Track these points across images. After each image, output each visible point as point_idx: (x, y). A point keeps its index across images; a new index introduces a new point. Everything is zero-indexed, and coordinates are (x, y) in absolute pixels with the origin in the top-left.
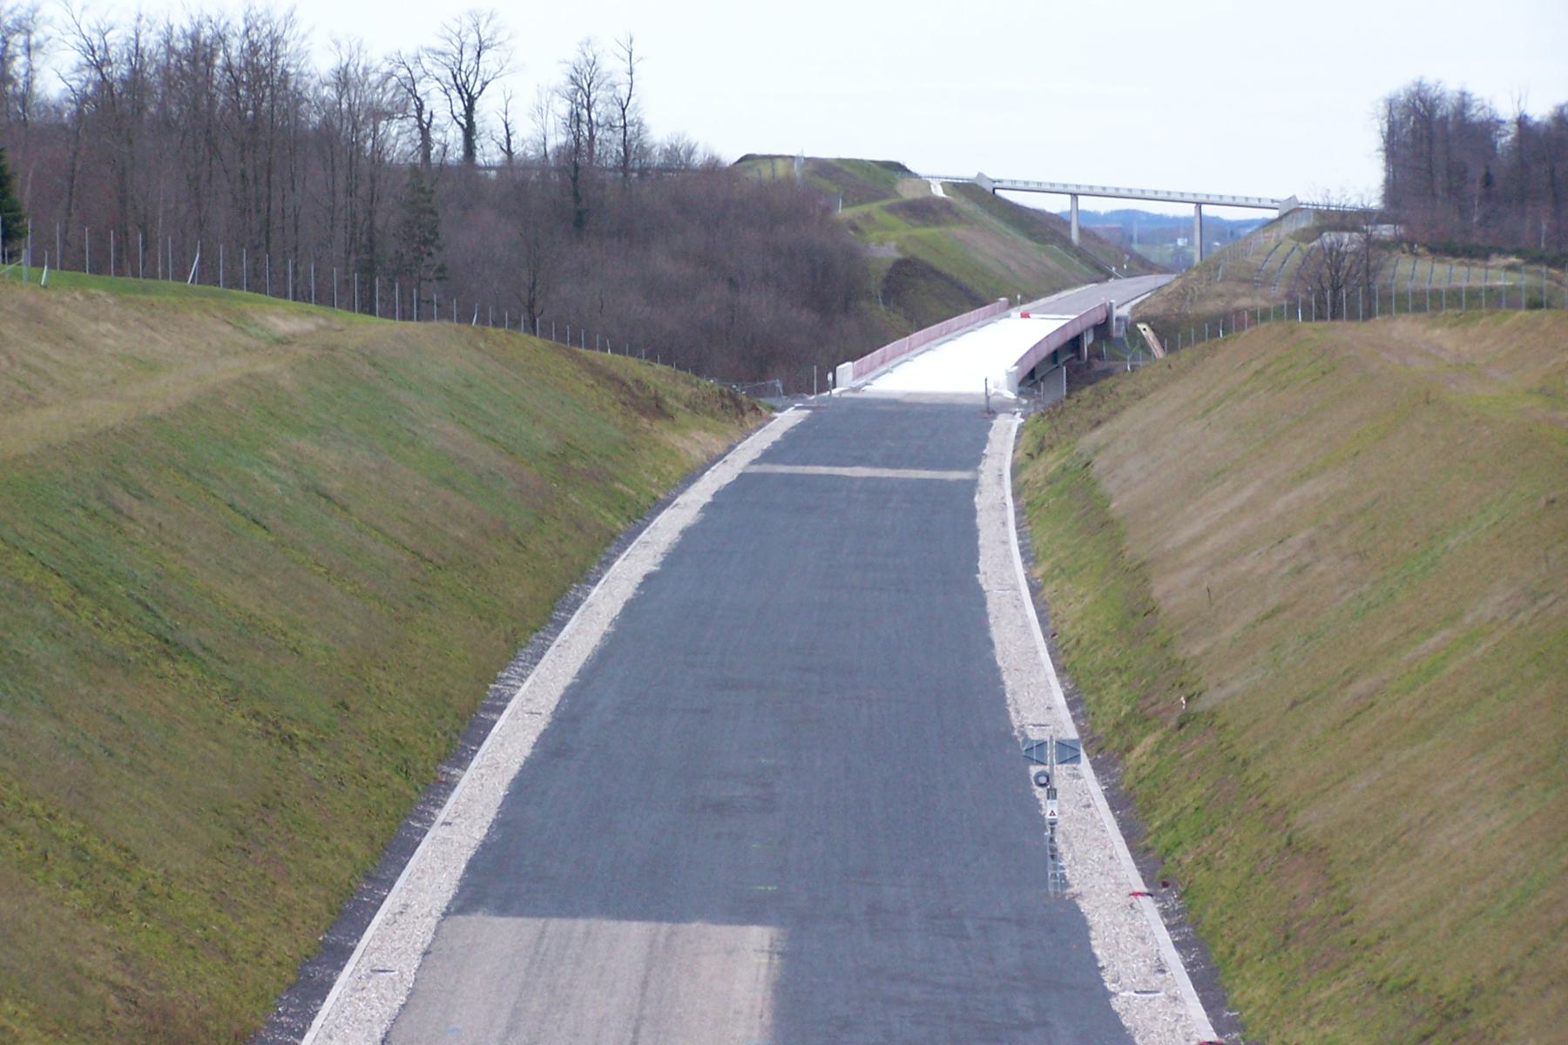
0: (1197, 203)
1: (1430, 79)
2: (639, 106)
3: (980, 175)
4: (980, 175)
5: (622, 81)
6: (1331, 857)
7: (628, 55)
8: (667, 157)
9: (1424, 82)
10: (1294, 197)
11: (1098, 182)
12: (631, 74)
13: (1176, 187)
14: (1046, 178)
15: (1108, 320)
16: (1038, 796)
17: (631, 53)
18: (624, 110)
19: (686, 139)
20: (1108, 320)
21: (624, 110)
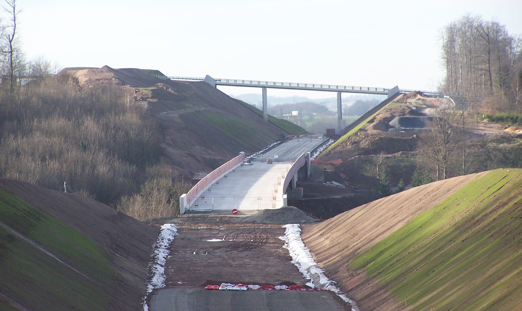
0: (339, 92)
1: (472, 16)
2: (20, 40)
3: (208, 77)
4: (208, 77)
5: (10, 25)
6: (18, 61)
7: (13, 8)
8: (33, 70)
9: (470, 17)
10: (397, 87)
11: (279, 80)
12: (15, 21)
13: (326, 82)
14: (247, 78)
15: (306, 163)
16: (136, 219)
17: (14, 8)
18: (10, 42)
19: (44, 59)
20: (306, 163)
21: (10, 42)
